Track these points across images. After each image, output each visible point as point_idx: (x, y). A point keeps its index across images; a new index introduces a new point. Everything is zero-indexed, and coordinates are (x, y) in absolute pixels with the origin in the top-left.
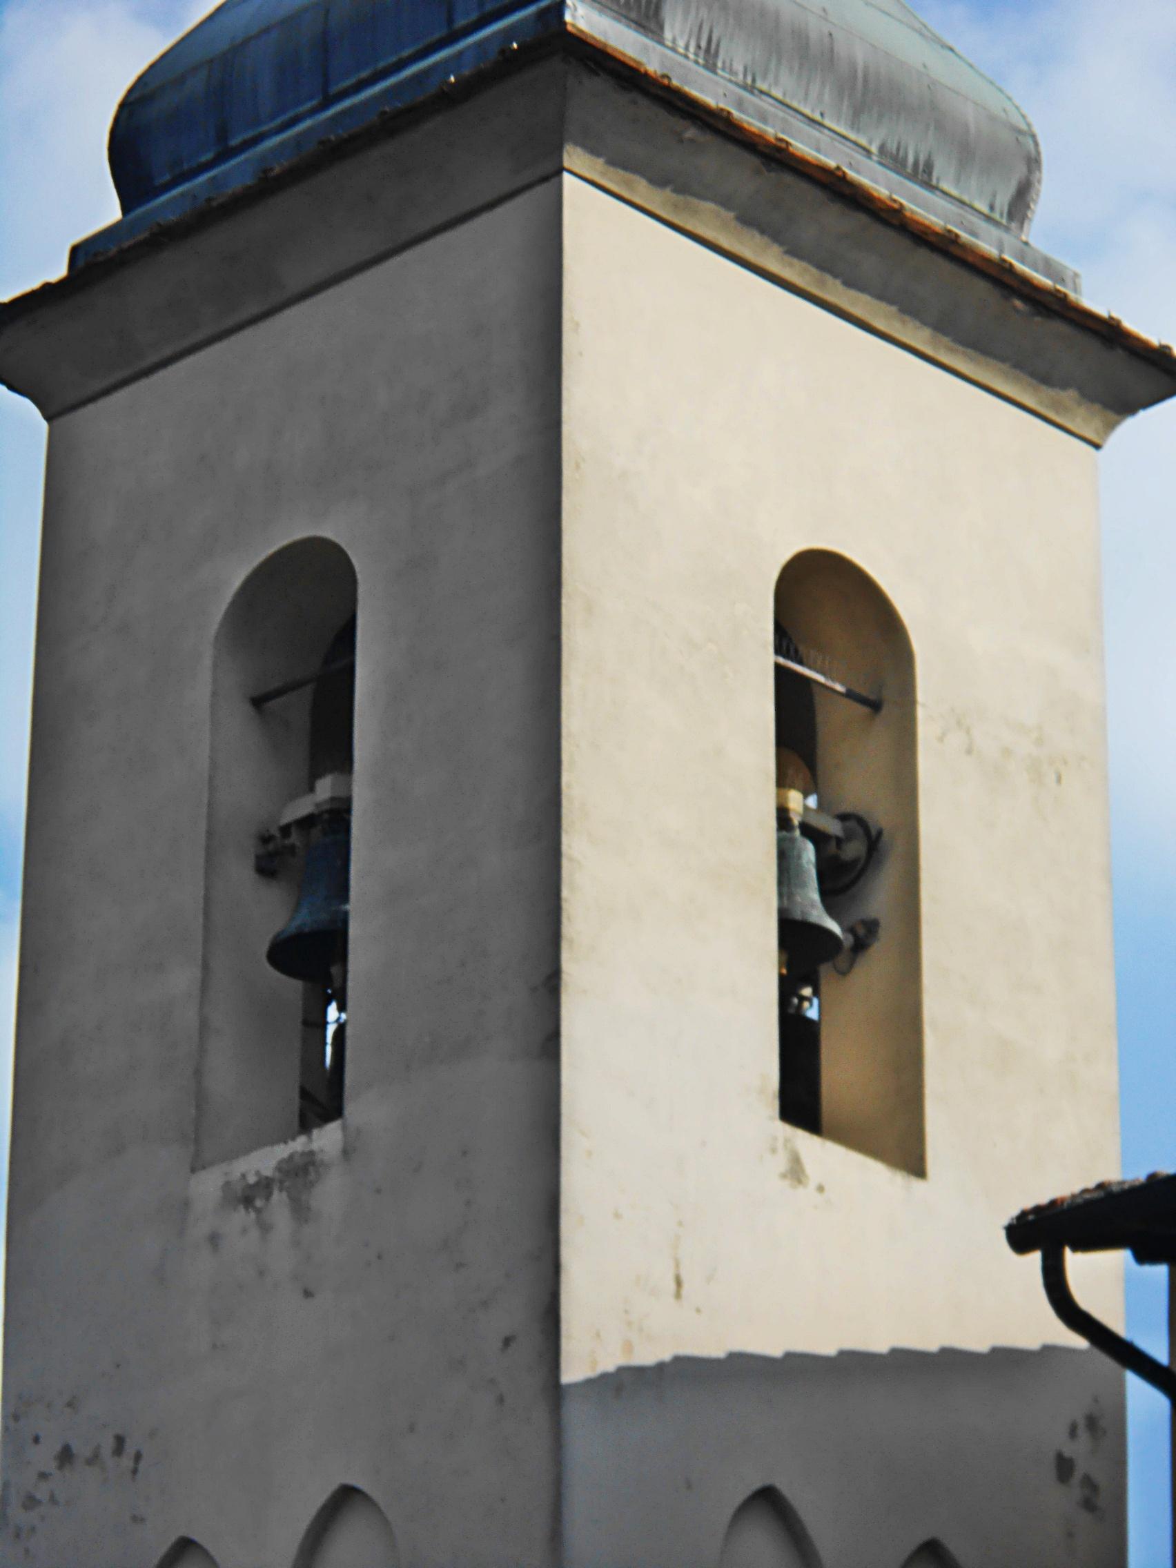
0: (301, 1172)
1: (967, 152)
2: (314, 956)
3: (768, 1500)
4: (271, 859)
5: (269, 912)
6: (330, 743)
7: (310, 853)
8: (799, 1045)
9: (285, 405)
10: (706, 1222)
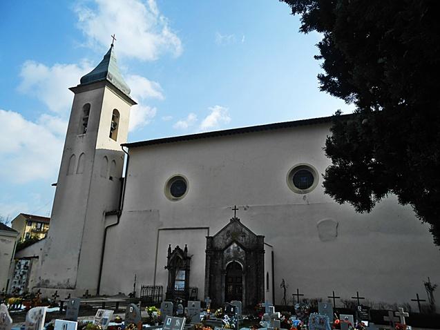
0: (83, 136)
1: (127, 90)
2: (85, 125)
3: (106, 157)
4: (84, 120)
5: (83, 122)
6: (88, 114)
7: (86, 119)
8: (111, 134)
9: (89, 96)
10: (104, 141)
